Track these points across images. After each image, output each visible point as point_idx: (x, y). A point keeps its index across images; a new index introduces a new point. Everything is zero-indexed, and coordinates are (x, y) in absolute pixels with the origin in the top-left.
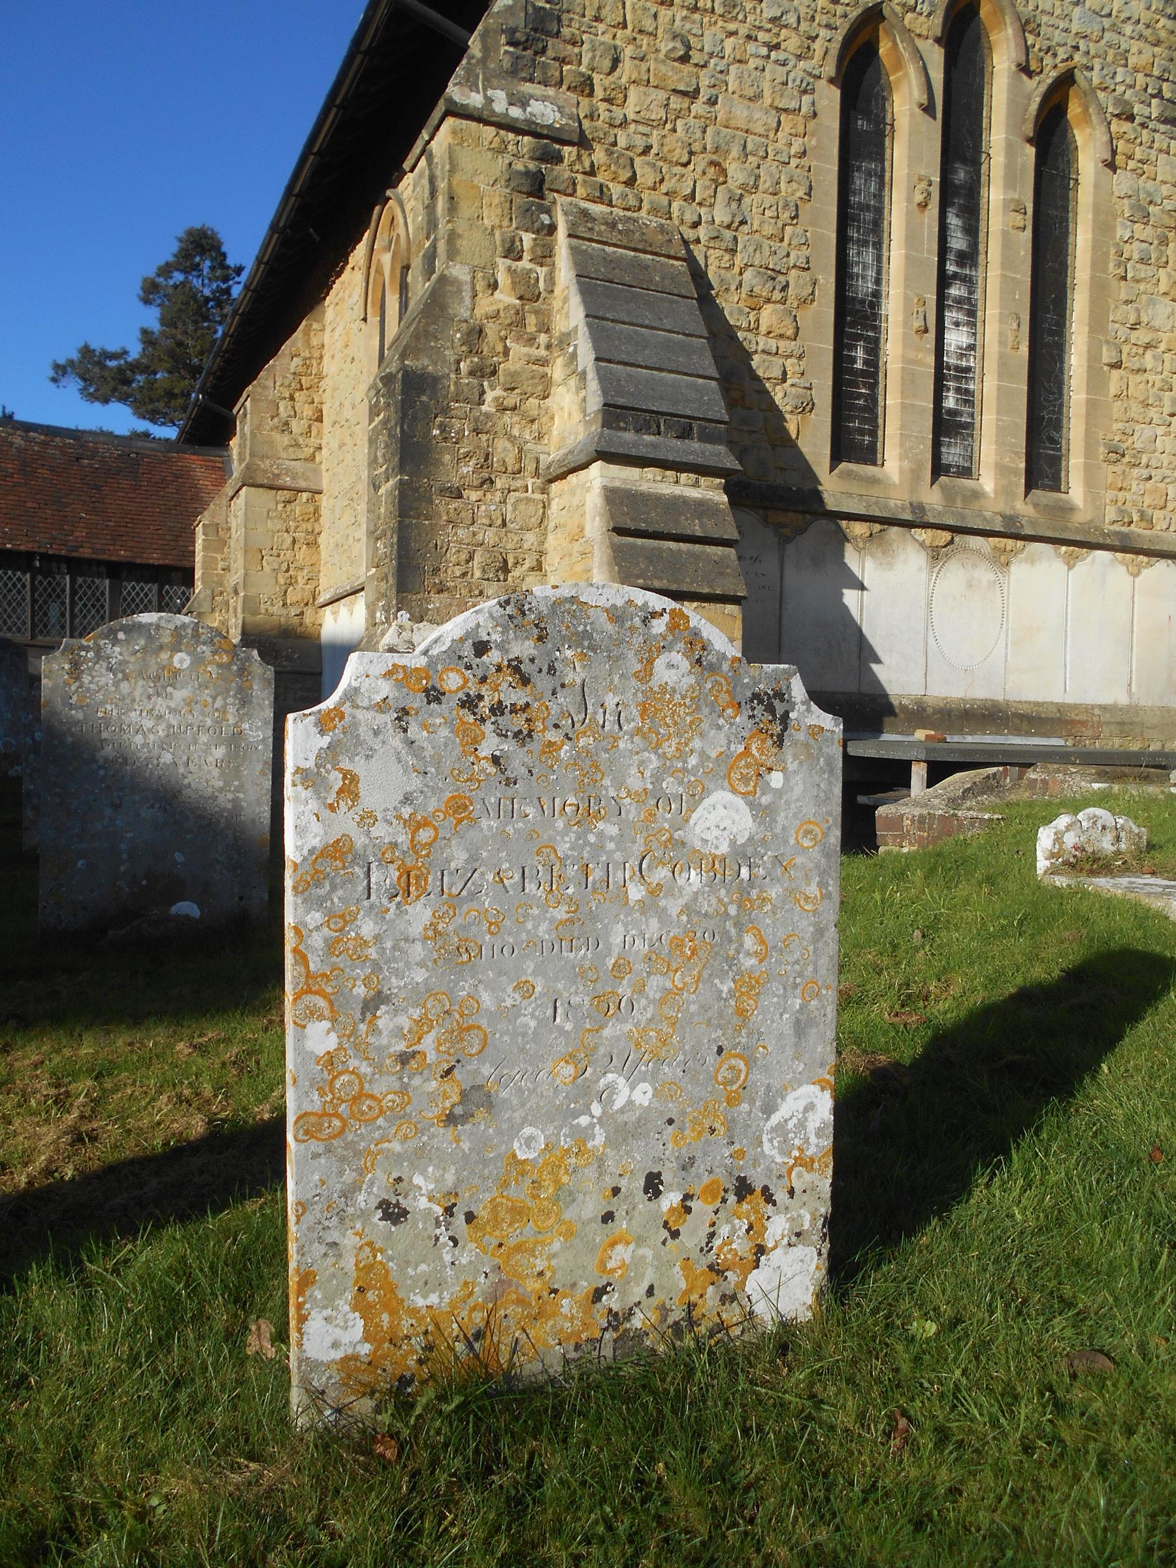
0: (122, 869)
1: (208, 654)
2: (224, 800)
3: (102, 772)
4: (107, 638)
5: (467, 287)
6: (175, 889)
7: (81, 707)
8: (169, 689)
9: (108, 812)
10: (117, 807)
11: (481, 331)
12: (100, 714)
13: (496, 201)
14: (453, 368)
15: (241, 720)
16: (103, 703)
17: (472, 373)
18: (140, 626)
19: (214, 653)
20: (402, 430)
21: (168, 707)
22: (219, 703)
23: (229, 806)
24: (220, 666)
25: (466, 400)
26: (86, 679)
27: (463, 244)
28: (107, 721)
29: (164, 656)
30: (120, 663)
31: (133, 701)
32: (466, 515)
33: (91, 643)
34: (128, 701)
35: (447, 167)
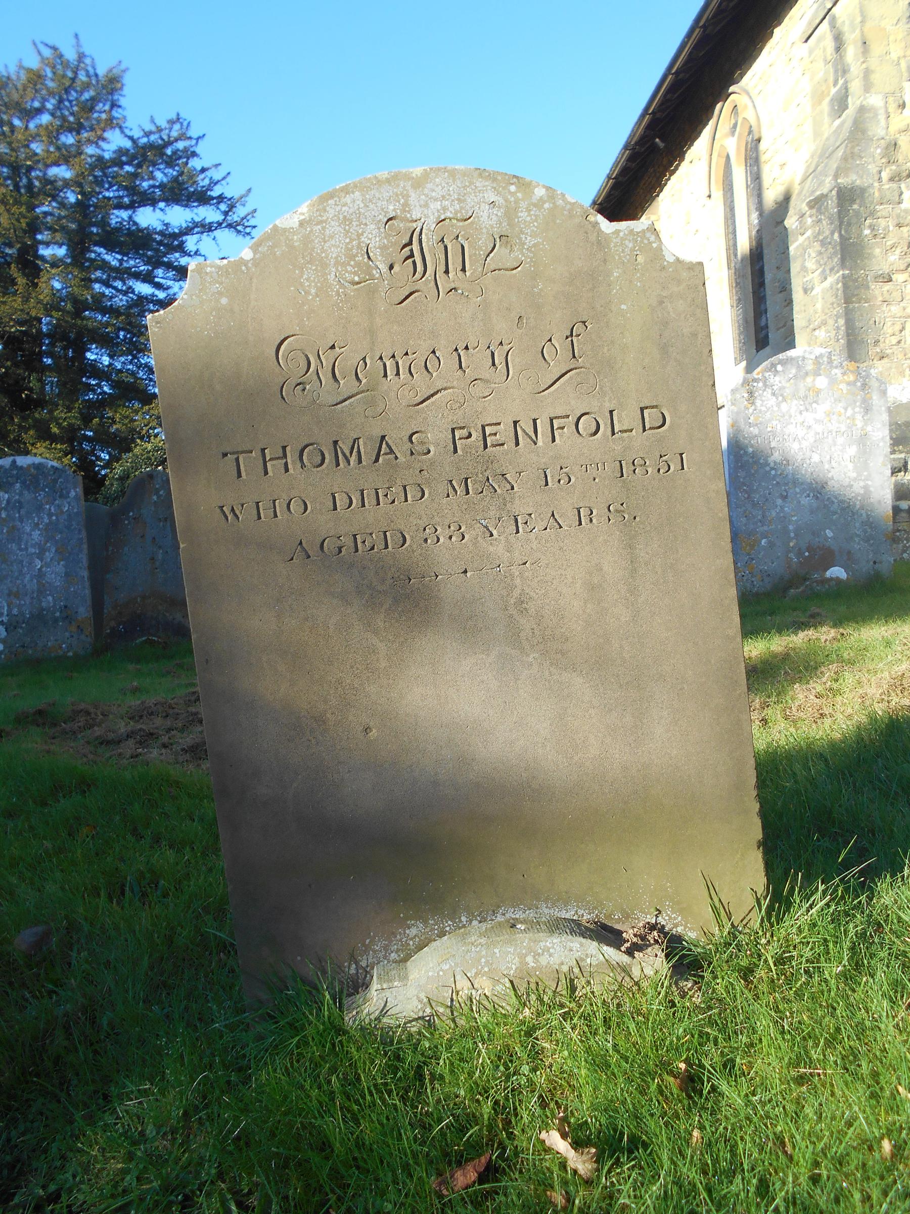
0: (791, 544)
1: (839, 375)
2: (858, 488)
3: (773, 472)
4: (770, 370)
5: (882, 111)
6: (827, 558)
7: (756, 425)
8: (814, 405)
9: (779, 502)
10: (784, 498)
11: (895, 144)
12: (769, 429)
13: (900, 36)
14: (877, 178)
15: (866, 424)
16: (770, 420)
17: (891, 179)
18: (792, 359)
19: (844, 374)
20: (841, 236)
21: (815, 419)
22: (850, 412)
23: (862, 492)
24: (849, 384)
25: (889, 202)
26: (758, 403)
27: (875, 78)
28: (774, 433)
29: (809, 379)
30: (780, 389)
31: (790, 416)
32: (897, 295)
33: (760, 376)
34: (787, 417)
35: (859, 19)
